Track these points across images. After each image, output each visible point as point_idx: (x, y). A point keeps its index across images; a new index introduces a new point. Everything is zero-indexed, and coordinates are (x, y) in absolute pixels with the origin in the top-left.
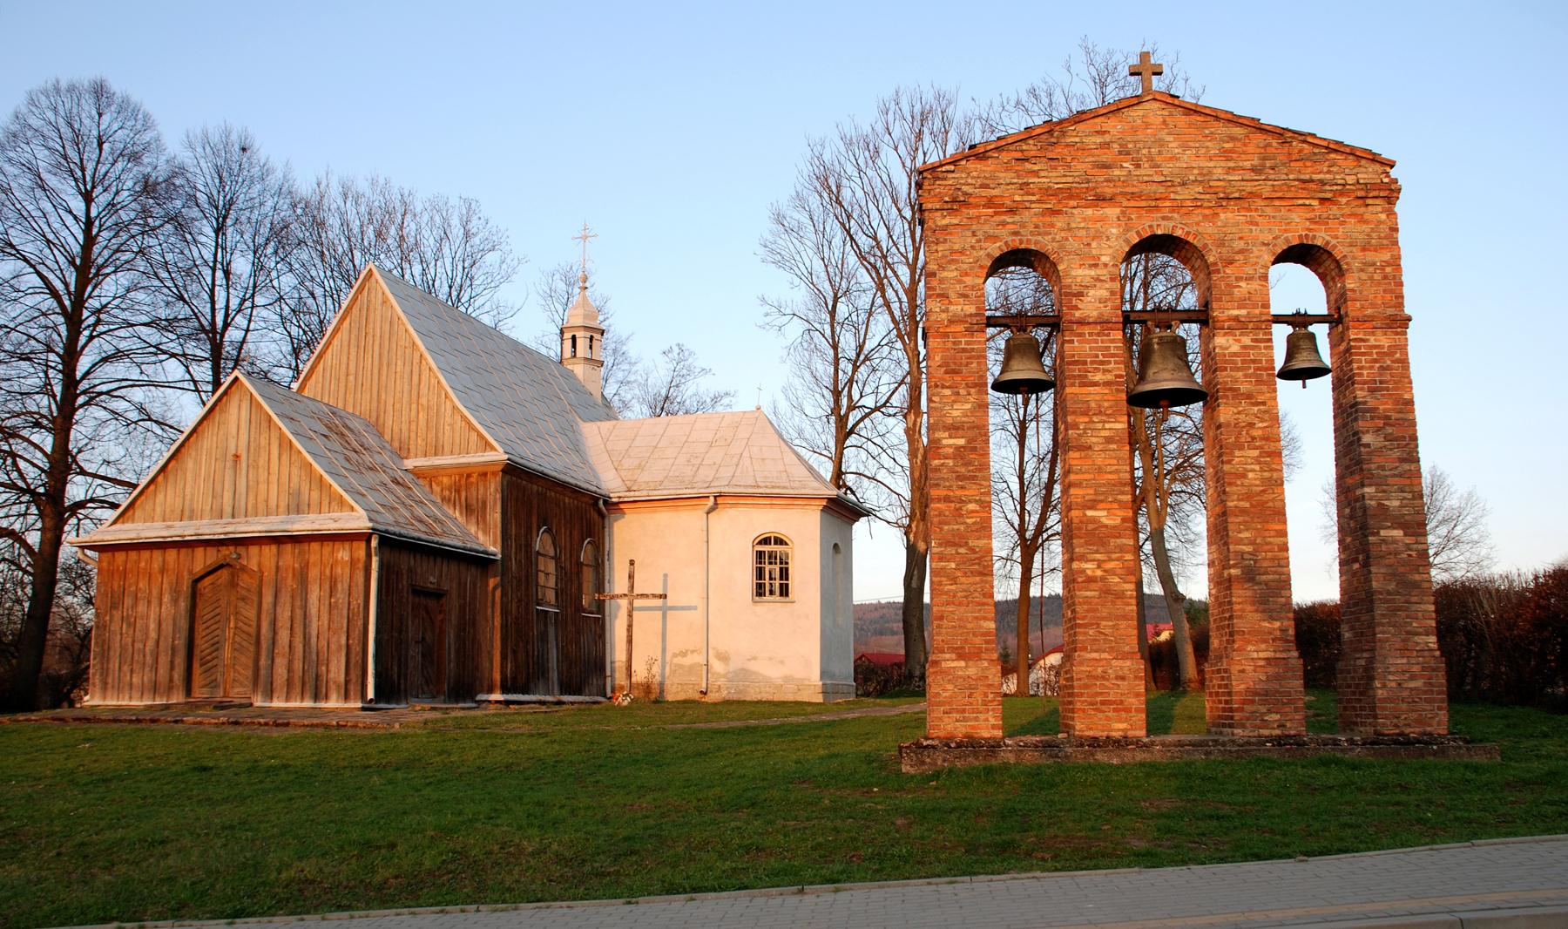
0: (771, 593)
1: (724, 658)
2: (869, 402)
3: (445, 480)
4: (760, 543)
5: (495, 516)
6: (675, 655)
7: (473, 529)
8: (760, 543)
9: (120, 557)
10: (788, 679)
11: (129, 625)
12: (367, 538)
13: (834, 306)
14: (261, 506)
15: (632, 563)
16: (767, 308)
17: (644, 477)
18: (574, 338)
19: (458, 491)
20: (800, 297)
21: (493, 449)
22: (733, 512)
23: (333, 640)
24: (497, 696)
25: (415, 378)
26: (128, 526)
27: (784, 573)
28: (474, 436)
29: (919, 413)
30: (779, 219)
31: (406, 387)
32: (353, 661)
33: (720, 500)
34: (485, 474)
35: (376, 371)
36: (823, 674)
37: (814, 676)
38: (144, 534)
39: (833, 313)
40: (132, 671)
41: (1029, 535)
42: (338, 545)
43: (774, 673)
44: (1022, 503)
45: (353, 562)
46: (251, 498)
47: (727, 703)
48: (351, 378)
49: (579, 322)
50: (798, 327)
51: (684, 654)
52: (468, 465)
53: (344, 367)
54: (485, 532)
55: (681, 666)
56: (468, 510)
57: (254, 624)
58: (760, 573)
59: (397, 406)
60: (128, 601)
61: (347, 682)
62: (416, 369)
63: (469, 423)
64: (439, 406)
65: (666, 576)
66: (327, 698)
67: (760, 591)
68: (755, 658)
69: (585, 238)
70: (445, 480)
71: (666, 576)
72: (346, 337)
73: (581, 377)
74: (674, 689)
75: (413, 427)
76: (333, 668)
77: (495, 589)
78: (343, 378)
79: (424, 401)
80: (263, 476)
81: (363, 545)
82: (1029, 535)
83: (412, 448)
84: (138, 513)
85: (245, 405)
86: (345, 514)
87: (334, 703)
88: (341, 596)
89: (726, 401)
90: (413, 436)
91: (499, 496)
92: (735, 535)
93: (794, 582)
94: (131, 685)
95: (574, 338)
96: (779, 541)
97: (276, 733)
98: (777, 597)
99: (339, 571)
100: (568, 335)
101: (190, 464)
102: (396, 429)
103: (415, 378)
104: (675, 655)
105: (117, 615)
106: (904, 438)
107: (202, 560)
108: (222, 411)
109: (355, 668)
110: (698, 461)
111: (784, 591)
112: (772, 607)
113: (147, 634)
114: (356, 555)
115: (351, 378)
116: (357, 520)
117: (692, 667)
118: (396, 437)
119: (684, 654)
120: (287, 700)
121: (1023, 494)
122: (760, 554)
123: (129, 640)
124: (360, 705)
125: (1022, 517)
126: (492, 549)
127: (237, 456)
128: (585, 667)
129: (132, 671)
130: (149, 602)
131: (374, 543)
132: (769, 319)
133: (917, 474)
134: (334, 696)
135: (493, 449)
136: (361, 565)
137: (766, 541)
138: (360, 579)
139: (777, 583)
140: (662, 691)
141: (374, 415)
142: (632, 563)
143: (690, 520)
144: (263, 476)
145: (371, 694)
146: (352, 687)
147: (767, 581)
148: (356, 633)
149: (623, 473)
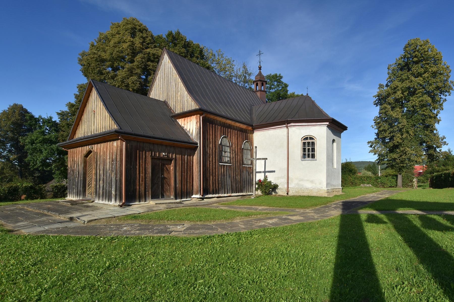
0: (308, 157)
4: (304, 139)
8: (304, 139)
27: (313, 150)
36: (328, 184)
37: (324, 187)
40: (187, 123)
48: (161, 89)
58: (304, 150)
65: (274, 171)
67: (304, 156)
71: (274, 171)
93: (317, 153)
98: (311, 159)
103: (177, 85)
111: (313, 156)
112: (308, 162)
115: (161, 89)
122: (304, 144)
129: (187, 123)
137: (306, 139)
139: (311, 153)
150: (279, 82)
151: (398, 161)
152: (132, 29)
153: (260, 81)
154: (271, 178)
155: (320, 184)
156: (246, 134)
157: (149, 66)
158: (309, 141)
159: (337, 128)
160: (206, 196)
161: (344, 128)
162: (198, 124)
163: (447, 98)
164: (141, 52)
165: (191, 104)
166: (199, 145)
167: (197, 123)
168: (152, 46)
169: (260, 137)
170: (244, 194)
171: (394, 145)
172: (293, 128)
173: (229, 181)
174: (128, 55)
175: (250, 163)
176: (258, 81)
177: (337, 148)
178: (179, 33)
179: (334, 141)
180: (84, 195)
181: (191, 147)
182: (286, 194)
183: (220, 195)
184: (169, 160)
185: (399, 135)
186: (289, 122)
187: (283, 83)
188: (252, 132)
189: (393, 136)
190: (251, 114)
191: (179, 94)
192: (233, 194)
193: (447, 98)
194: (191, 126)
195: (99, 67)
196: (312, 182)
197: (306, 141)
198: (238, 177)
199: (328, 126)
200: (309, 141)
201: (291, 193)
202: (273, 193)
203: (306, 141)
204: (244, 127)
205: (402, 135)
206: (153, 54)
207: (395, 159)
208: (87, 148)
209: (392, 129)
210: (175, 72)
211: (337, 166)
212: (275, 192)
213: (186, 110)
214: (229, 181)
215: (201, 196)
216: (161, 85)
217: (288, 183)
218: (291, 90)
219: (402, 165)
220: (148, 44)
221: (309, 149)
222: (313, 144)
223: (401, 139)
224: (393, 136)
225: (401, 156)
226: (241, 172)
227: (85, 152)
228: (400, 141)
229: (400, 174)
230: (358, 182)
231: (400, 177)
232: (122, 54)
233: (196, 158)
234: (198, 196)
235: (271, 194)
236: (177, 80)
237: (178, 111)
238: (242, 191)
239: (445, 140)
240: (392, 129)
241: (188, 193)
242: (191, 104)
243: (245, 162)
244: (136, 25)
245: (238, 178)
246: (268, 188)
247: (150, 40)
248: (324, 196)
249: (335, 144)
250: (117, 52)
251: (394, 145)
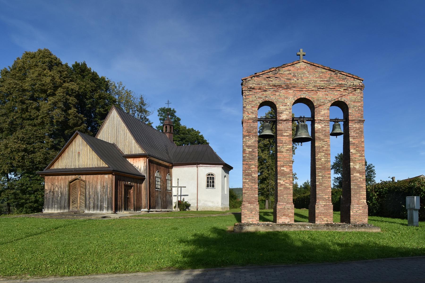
15: (178, 179)
27: (213, 182)
36: (222, 204)
48: (110, 134)
58: (208, 182)
61: (108, 207)
65: (188, 195)
67: (208, 186)
71: (188, 195)
96: (212, 175)
98: (212, 187)
103: (125, 135)
111: (213, 186)
112: (210, 190)
115: (110, 134)
122: (208, 178)
134: (105, 210)
137: (209, 175)
139: (212, 184)
142: (178, 179)
150: (173, 116)
151: (265, 190)
152: (49, 62)
153: (169, 125)
154: (186, 199)
155: (217, 203)
156: (168, 169)
157: (69, 100)
158: (211, 176)
159: (227, 168)
160: (150, 210)
161: (231, 168)
162: (146, 164)
163: (297, 146)
164: (61, 86)
165: (138, 150)
166: (146, 177)
167: (144, 163)
168: (69, 80)
169: (176, 171)
170: (168, 210)
171: (263, 178)
172: (201, 168)
173: (160, 201)
174: (50, 89)
175: (170, 189)
176: (167, 125)
177: (227, 181)
178: (85, 65)
179: (225, 176)
180: (69, 208)
181: (140, 179)
182: (196, 210)
183: (157, 210)
184: (131, 187)
185: (266, 171)
186: (199, 164)
187: (176, 117)
188: (172, 168)
189: (263, 171)
190: (168, 153)
191: (127, 140)
192: (163, 210)
193: (297, 146)
194: (140, 165)
195: (22, 97)
196: (213, 202)
197: (209, 176)
198: (161, 198)
199: (223, 168)
200: (211, 176)
201: (199, 210)
202: (187, 210)
203: (209, 176)
204: (167, 164)
205: (268, 171)
206: (71, 89)
207: (263, 188)
208: (74, 177)
209: (262, 166)
210: (123, 125)
211: (227, 193)
212: (189, 209)
213: (133, 153)
214: (160, 201)
215: (147, 210)
216: (110, 131)
217: (197, 203)
218: (183, 123)
219: (268, 193)
220: (64, 78)
221: (211, 181)
222: (213, 178)
223: (268, 174)
224: (263, 171)
225: (267, 186)
226: (166, 195)
227: (70, 180)
228: (267, 175)
229: (267, 199)
230: (238, 205)
231: (267, 201)
232: (43, 87)
233: (144, 186)
234: (146, 210)
235: (185, 210)
236: (125, 131)
237: (126, 153)
238: (166, 209)
239: (296, 176)
240: (262, 166)
241: (138, 208)
242: (138, 150)
243: (168, 189)
244: (52, 59)
245: (164, 199)
246: (184, 206)
247: (66, 74)
248: (220, 211)
249: (226, 178)
250: (40, 85)
251: (263, 178)
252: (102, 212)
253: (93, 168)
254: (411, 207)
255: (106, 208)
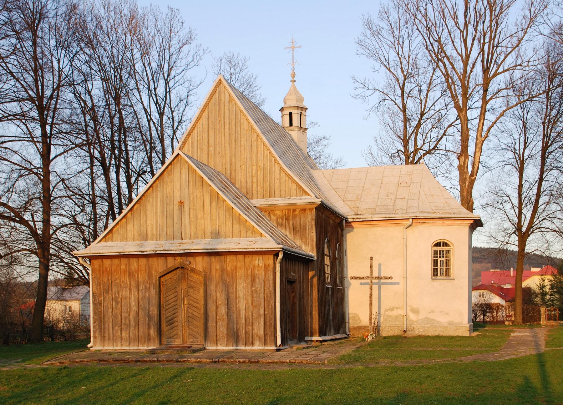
1: (416, 311)
2: (426, 147)
3: (279, 213)
4: (434, 246)
5: (312, 234)
6: (387, 310)
7: (298, 242)
8: (434, 246)
9: (107, 262)
10: (451, 323)
11: (117, 303)
12: (276, 254)
13: (404, 84)
14: (200, 233)
15: (371, 258)
16: (357, 85)
17: (179, 165)
18: (291, 114)
19: (288, 219)
20: (381, 78)
21: (307, 194)
22: (421, 227)
23: (255, 312)
24: (316, 338)
25: (254, 150)
26: (109, 243)
28: (294, 187)
29: (467, 156)
30: (369, 25)
31: (248, 155)
32: (268, 323)
33: (415, 221)
34: (305, 210)
35: (227, 145)
38: (127, 250)
39: (403, 90)
41: (524, 229)
42: (254, 257)
43: (443, 320)
44: (520, 212)
45: (266, 267)
46: (193, 228)
47: (419, 337)
48: (211, 148)
49: (294, 104)
50: (377, 96)
51: (392, 309)
52: (296, 205)
53: (206, 141)
54: (306, 244)
55: (390, 316)
56: (295, 230)
57: (202, 302)
58: (435, 263)
59: (243, 167)
60: (115, 289)
61: (265, 335)
62: (254, 144)
63: (291, 178)
64: (271, 167)
66: (253, 344)
67: (435, 273)
68: (433, 312)
69: (293, 48)
70: (279, 213)
72: (205, 123)
73: (296, 139)
74: (386, 329)
75: (255, 180)
76: (255, 327)
77: (313, 277)
78: (205, 148)
79: (260, 163)
80: (200, 215)
81: (272, 257)
82: (524, 229)
83: (255, 193)
84: (115, 235)
85: (185, 171)
86: (257, 239)
87: (257, 347)
88: (258, 285)
89: (324, 142)
90: (255, 185)
91: (314, 223)
92: (423, 239)
94: (121, 338)
95: (291, 114)
96: (445, 244)
97: (253, 367)
99: (257, 272)
100: (287, 112)
101: (149, 207)
102: (243, 181)
103: (254, 150)
104: (387, 310)
105: (109, 297)
106: (518, 188)
107: (159, 266)
108: (168, 175)
109: (269, 326)
110: (394, 196)
111: (448, 274)
112: (441, 283)
113: (130, 308)
114: (267, 263)
115: (211, 148)
116: (271, 245)
117: (397, 317)
118: (244, 186)
119: (392, 309)
120: (227, 345)
121: (520, 204)
122: (435, 252)
123: (119, 312)
124: (275, 348)
125: (519, 218)
126: (311, 253)
127: (181, 203)
128: (334, 318)
130: (130, 289)
131: (281, 256)
132: (358, 92)
133: (465, 194)
134: (257, 343)
135: (307, 194)
136: (271, 269)
137: (438, 244)
138: (271, 277)
139: (444, 268)
140: (377, 329)
141: (228, 172)
142: (371, 258)
143: (395, 232)
144: (200, 215)
145: (279, 342)
146: (268, 338)
147: (439, 268)
148: (269, 309)
149: (349, 203)
158: (442, 248)
197: (438, 248)
252: (247, 348)
253: (519, 240)
254: (245, 93)
255: (260, 338)
